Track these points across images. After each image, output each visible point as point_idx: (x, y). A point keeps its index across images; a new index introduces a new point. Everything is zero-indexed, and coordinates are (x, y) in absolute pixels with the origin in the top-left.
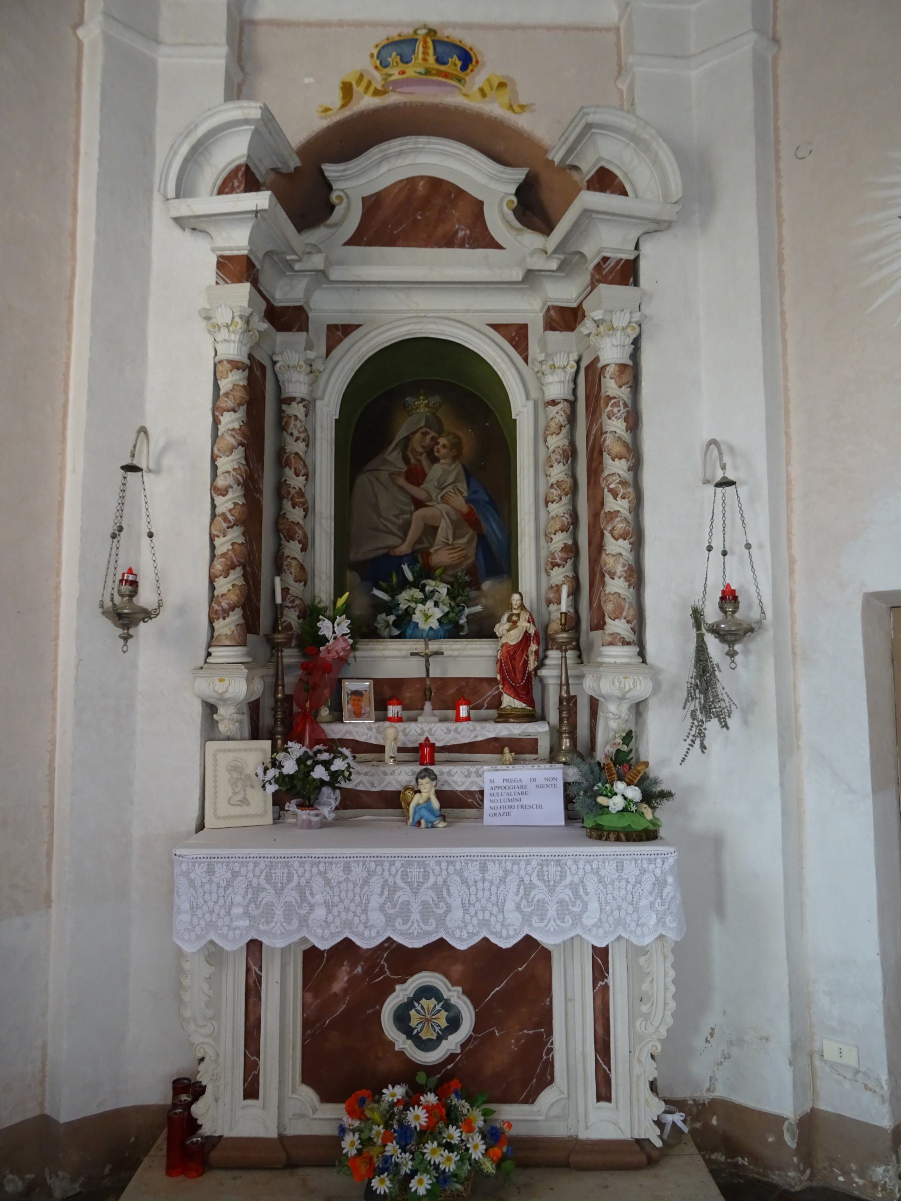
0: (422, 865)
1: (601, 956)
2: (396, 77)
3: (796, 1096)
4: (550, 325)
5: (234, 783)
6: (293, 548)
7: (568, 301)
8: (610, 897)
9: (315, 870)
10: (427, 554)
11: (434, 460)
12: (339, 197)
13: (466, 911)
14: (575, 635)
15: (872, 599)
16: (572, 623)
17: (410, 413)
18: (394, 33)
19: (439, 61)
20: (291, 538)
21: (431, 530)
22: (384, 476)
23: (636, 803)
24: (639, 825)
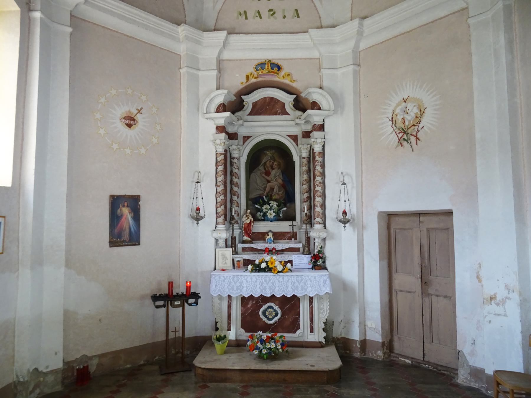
1: (311, 299)
3: (360, 335)
4: (304, 137)
5: (223, 259)
6: (235, 198)
11: (273, 169)
14: (309, 220)
15: (380, 214)
17: (266, 155)
18: (260, 62)
19: (272, 69)
20: (235, 195)
21: (272, 189)
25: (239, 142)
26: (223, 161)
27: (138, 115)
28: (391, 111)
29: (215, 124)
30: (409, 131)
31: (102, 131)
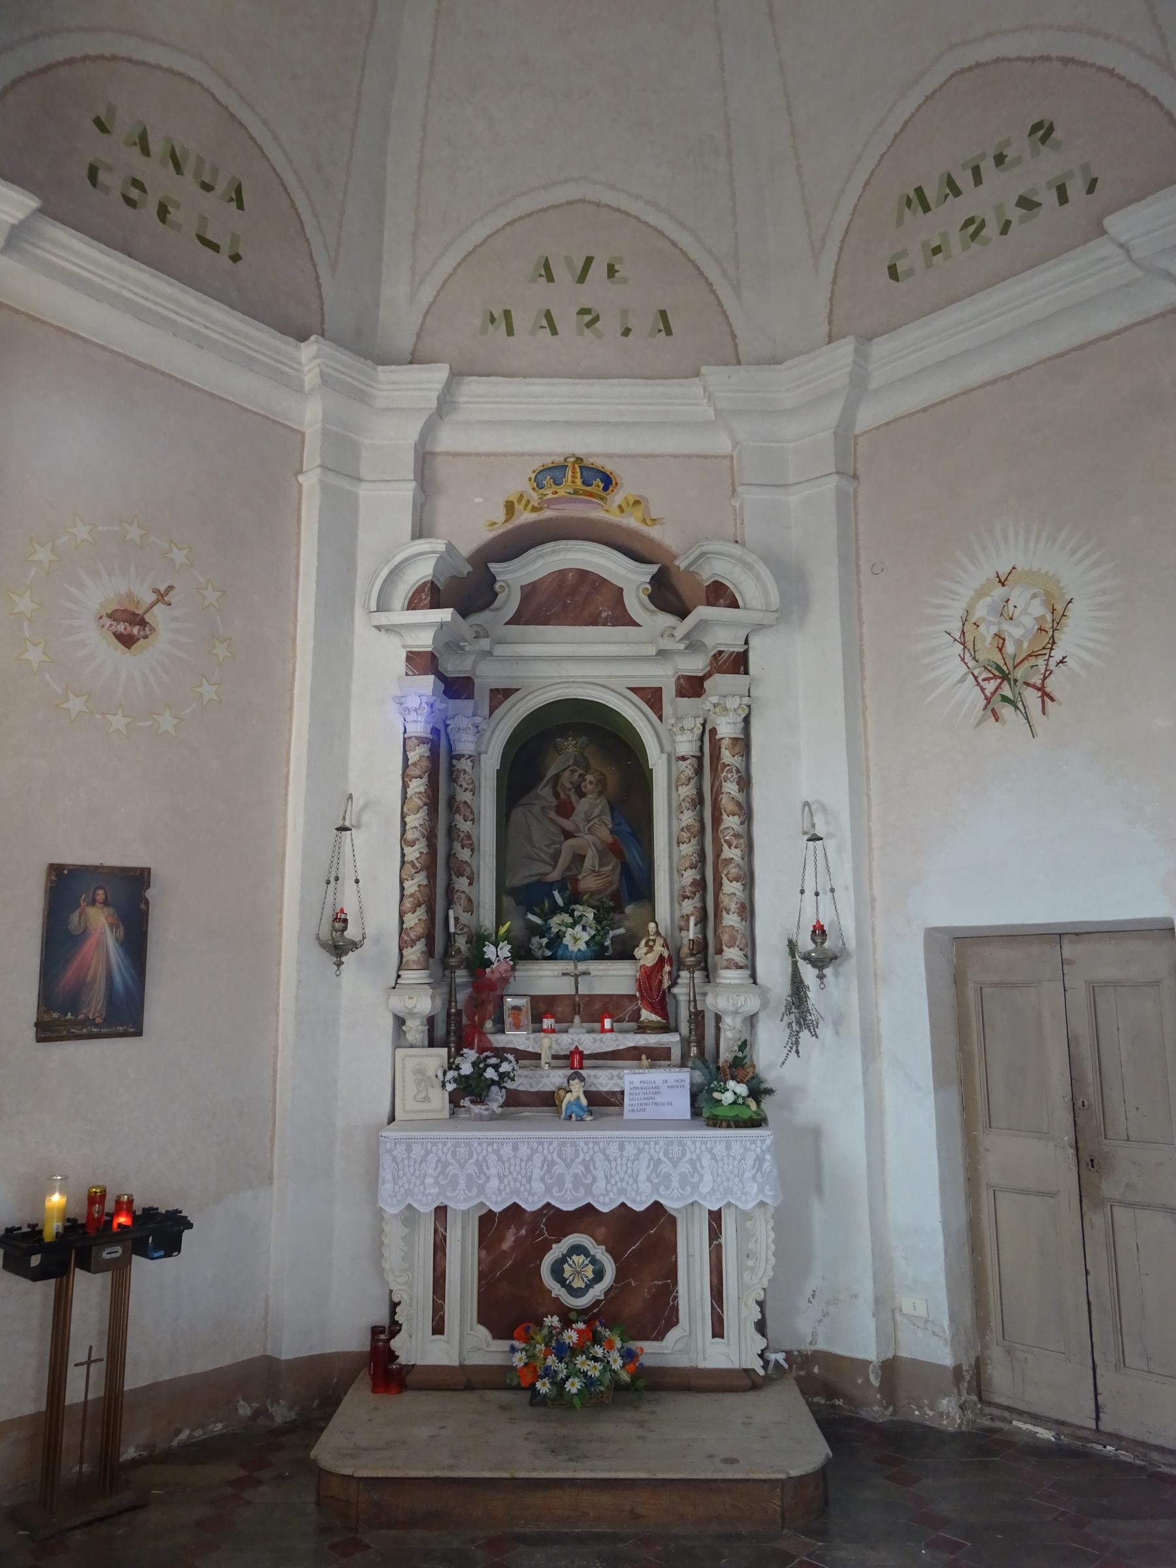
0: (574, 1144)
1: (715, 1217)
2: (550, 496)
3: (878, 1343)
4: (681, 693)
5: (418, 1083)
6: (462, 883)
7: (696, 671)
8: (720, 1171)
9: (490, 1149)
10: (575, 881)
11: (582, 795)
12: (501, 587)
13: (608, 1182)
14: (704, 957)
15: (932, 934)
16: (701, 948)
17: (559, 751)
18: (548, 461)
19: (584, 483)
20: (460, 874)
21: (579, 859)
22: (537, 809)
23: (744, 1098)
24: (745, 1114)
25: (476, 708)
26: (425, 764)
27: (159, 609)
28: (959, 613)
29: (404, 647)
30: (1019, 674)
31: (34, 655)
